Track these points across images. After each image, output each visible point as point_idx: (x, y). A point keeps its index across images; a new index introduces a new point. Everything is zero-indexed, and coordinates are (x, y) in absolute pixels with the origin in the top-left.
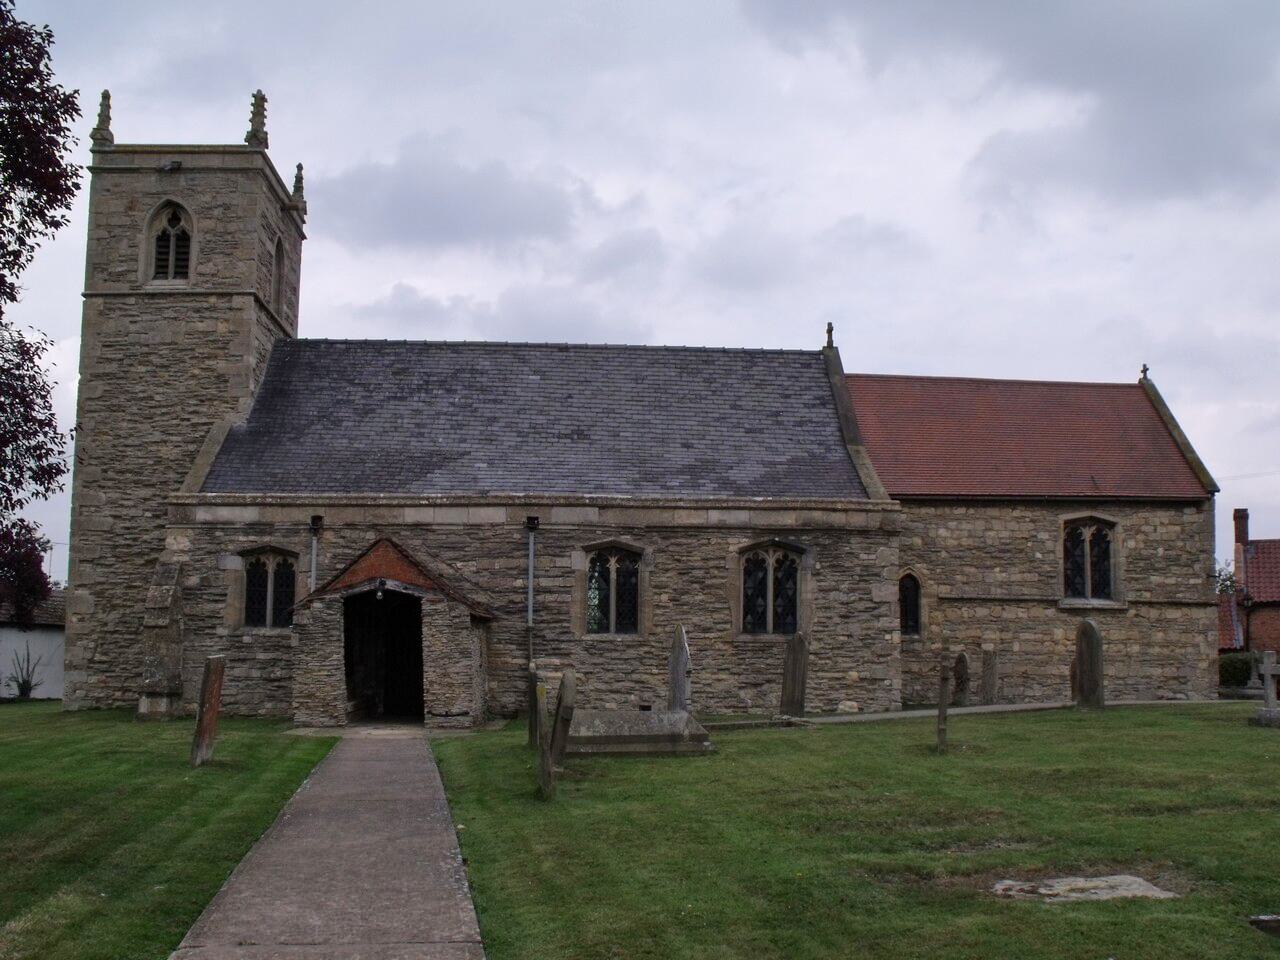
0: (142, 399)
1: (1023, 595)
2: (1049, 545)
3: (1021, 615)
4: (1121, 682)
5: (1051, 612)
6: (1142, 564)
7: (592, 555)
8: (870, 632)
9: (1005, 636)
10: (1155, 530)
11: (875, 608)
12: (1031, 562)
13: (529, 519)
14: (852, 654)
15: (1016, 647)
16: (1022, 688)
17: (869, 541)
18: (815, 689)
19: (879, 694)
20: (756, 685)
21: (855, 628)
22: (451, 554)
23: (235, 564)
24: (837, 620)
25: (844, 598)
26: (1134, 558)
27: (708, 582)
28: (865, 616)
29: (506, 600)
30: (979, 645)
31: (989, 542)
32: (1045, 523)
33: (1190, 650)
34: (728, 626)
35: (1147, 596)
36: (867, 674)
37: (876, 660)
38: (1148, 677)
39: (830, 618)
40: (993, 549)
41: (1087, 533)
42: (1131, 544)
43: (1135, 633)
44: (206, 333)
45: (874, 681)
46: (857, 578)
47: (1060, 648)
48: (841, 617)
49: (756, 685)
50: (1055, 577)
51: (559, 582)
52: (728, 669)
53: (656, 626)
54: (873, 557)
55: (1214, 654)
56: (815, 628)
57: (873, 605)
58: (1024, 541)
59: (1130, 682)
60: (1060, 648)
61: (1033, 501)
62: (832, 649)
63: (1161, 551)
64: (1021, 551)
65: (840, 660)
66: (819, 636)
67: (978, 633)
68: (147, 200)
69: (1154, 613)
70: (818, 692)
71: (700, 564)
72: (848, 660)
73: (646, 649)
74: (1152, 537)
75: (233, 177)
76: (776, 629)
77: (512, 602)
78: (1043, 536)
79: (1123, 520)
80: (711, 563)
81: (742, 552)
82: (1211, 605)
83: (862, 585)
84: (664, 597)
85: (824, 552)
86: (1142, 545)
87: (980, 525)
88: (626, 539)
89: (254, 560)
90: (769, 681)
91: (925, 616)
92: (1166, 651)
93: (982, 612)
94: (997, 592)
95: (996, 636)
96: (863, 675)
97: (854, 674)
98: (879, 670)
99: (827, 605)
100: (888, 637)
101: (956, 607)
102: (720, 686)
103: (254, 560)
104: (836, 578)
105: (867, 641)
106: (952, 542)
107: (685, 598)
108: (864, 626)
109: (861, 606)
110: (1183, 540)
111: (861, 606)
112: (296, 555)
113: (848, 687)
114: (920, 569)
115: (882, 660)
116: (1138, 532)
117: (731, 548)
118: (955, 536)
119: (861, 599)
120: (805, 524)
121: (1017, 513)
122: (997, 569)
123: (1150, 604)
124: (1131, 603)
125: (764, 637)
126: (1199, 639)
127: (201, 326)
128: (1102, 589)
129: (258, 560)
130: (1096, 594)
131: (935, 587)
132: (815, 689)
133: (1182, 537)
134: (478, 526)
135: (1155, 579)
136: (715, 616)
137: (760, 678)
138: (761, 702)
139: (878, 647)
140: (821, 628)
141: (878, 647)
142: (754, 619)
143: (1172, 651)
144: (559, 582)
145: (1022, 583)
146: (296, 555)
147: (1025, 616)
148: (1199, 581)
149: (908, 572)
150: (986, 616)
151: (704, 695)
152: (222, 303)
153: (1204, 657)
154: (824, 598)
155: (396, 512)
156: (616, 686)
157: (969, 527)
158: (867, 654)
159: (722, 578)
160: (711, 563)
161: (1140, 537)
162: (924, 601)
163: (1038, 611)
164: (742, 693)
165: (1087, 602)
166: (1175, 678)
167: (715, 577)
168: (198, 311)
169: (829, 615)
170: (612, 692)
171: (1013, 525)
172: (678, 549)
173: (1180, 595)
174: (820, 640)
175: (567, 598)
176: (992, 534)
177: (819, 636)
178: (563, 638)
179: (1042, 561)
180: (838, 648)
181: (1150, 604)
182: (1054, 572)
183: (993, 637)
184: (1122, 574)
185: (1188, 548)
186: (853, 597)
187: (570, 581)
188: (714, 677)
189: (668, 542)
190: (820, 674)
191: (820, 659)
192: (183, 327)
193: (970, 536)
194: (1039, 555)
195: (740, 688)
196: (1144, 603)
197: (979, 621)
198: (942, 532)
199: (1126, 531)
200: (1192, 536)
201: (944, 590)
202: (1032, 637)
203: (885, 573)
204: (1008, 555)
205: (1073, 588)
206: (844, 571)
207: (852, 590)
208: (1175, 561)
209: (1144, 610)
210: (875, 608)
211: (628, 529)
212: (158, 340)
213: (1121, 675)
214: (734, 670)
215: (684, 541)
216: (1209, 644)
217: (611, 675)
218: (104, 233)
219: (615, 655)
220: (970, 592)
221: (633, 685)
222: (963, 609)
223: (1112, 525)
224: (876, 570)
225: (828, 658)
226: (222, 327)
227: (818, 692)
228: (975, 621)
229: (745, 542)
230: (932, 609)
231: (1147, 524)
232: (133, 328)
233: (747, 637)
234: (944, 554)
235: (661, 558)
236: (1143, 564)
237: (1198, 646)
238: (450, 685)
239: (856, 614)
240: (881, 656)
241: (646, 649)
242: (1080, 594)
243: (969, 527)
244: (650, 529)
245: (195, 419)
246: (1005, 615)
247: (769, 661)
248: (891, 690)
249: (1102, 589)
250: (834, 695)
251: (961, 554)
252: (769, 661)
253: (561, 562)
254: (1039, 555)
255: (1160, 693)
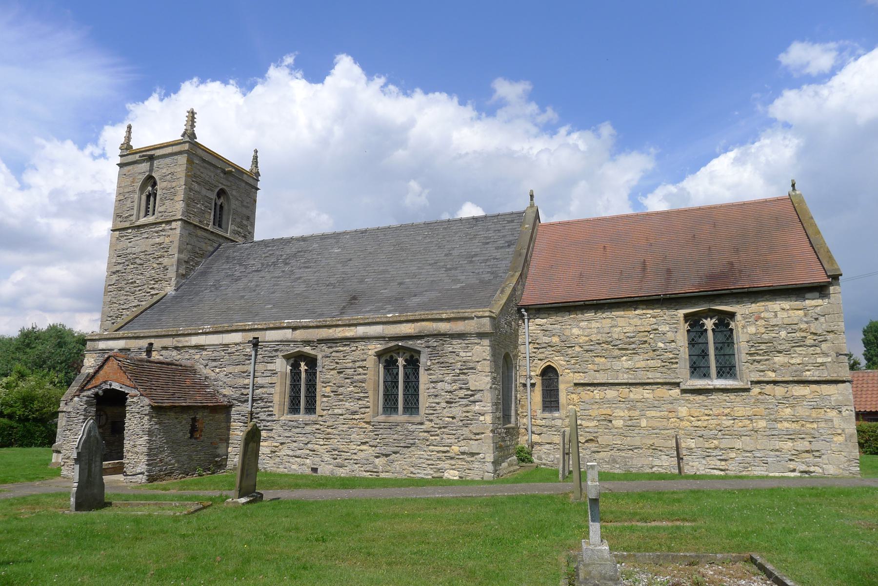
0: (132, 283)
1: (648, 378)
2: (670, 336)
3: (646, 396)
4: (749, 454)
5: (676, 392)
6: (763, 347)
7: (292, 361)
8: (468, 414)
9: (632, 413)
10: (776, 316)
11: (472, 395)
12: (654, 351)
13: (254, 338)
14: (454, 432)
15: (644, 423)
16: (651, 459)
17: (466, 342)
18: (428, 460)
19: (476, 465)
20: (387, 455)
21: (457, 411)
22: (215, 364)
23: (281, 366)
24: (444, 405)
25: (448, 387)
26: (755, 342)
27: (356, 378)
28: (465, 402)
29: (240, 392)
30: (611, 421)
31: (616, 336)
32: (665, 317)
33: (823, 425)
34: (368, 410)
35: (772, 376)
36: (465, 449)
37: (473, 437)
38: (777, 450)
39: (438, 403)
40: (619, 342)
41: (709, 323)
42: (752, 329)
43: (761, 410)
44: (160, 244)
45: (473, 454)
46: (458, 371)
47: (685, 424)
48: (447, 402)
49: (387, 455)
50: (677, 363)
51: (268, 380)
52: (367, 442)
53: (324, 410)
54: (468, 354)
55: (851, 427)
56: (427, 412)
57: (469, 393)
58: (646, 333)
59: (758, 455)
60: (685, 424)
61: (576, 306)
62: (440, 428)
63: (783, 334)
64: (645, 342)
65: (445, 436)
66: (431, 417)
67: (609, 411)
68: (140, 177)
69: (779, 390)
70: (429, 462)
71: (350, 365)
72: (451, 436)
73: (318, 426)
74: (774, 321)
75: (176, 157)
76: (404, 412)
77: (242, 394)
78: (664, 328)
79: (741, 310)
80: (358, 364)
81: (379, 355)
82: (843, 382)
83: (462, 377)
84: (328, 389)
85: (434, 353)
86: (763, 330)
87: (607, 323)
88: (307, 349)
89: (388, 358)
90: (395, 453)
91: (563, 397)
92: (794, 426)
93: (611, 393)
94: (624, 378)
95: (626, 413)
96: (463, 449)
97: (455, 448)
98: (474, 446)
99: (436, 393)
100: (482, 418)
101: (589, 390)
102: (361, 455)
103: (388, 358)
104: (442, 372)
105: (466, 422)
106: (582, 339)
107: (341, 390)
108: (464, 409)
109: (462, 393)
110: (807, 323)
111: (462, 393)
112: (419, 352)
113: (452, 458)
114: (558, 362)
115: (478, 437)
116: (759, 318)
117: (370, 352)
118: (586, 334)
119: (461, 388)
120: (420, 332)
121: (638, 312)
122: (624, 358)
123: (775, 383)
124: (752, 382)
125: (394, 418)
126: (833, 414)
127: (157, 240)
128: (727, 369)
129: (392, 357)
130: (720, 374)
131: (571, 374)
132: (428, 460)
133: (805, 319)
134: (227, 345)
135: (779, 359)
136: (360, 402)
137: (388, 450)
138: (389, 468)
139: (474, 428)
140: (432, 412)
141: (474, 428)
142: (390, 405)
143: (803, 426)
144: (268, 380)
145: (647, 369)
146: (419, 352)
147: (651, 396)
148: (829, 360)
149: (548, 364)
150: (615, 397)
151: (352, 461)
152: (168, 227)
153: (840, 431)
154: (434, 388)
155: (187, 338)
156: (299, 453)
157: (598, 325)
158: (466, 431)
159: (365, 374)
160: (358, 364)
161: (761, 322)
162: (562, 387)
163: (662, 392)
164: (377, 461)
165: (710, 382)
166: (807, 452)
167: (360, 374)
168: (157, 232)
169: (437, 401)
170: (296, 457)
171: (636, 321)
172: (338, 354)
173: (808, 373)
174: (431, 421)
175: (272, 390)
176: (618, 330)
177: (431, 417)
178: (270, 418)
179: (665, 350)
180: (444, 427)
181: (775, 383)
182: (676, 358)
183: (622, 414)
184: (744, 357)
185: (813, 330)
186: (456, 386)
187: (274, 379)
188: (358, 448)
189: (331, 350)
190: (431, 448)
191: (432, 436)
192: (151, 241)
193: (599, 333)
194: (661, 345)
195: (377, 457)
196: (768, 383)
197: (609, 401)
198: (575, 331)
199: (744, 318)
200: (816, 319)
201: (580, 378)
202: (659, 414)
203: (479, 367)
204: (633, 346)
205: (698, 368)
206: (448, 366)
207: (455, 381)
208: (800, 343)
209: (768, 388)
210: (472, 396)
211: (307, 343)
212: (139, 250)
213: (748, 449)
214: (371, 443)
215: (341, 349)
216: (845, 419)
217: (295, 444)
218: (122, 197)
219: (298, 430)
220: (601, 378)
221: (308, 452)
222: (595, 392)
223: (732, 315)
224: (472, 365)
225: (438, 435)
226: (167, 240)
227: (429, 462)
228: (603, 401)
229: (379, 347)
230: (569, 393)
231: (767, 311)
232: (130, 245)
233: (381, 418)
234: (577, 349)
235: (327, 362)
236: (764, 349)
237: (832, 421)
238: (137, 453)
239: (457, 400)
240: (476, 434)
241: (318, 426)
242: (706, 376)
243: (598, 325)
244: (321, 341)
245: (153, 292)
246: (632, 396)
247: (395, 437)
248: (484, 462)
249: (727, 369)
250: (442, 465)
251: (592, 347)
252: (395, 437)
253: (270, 367)
254: (661, 345)
255: (792, 465)
